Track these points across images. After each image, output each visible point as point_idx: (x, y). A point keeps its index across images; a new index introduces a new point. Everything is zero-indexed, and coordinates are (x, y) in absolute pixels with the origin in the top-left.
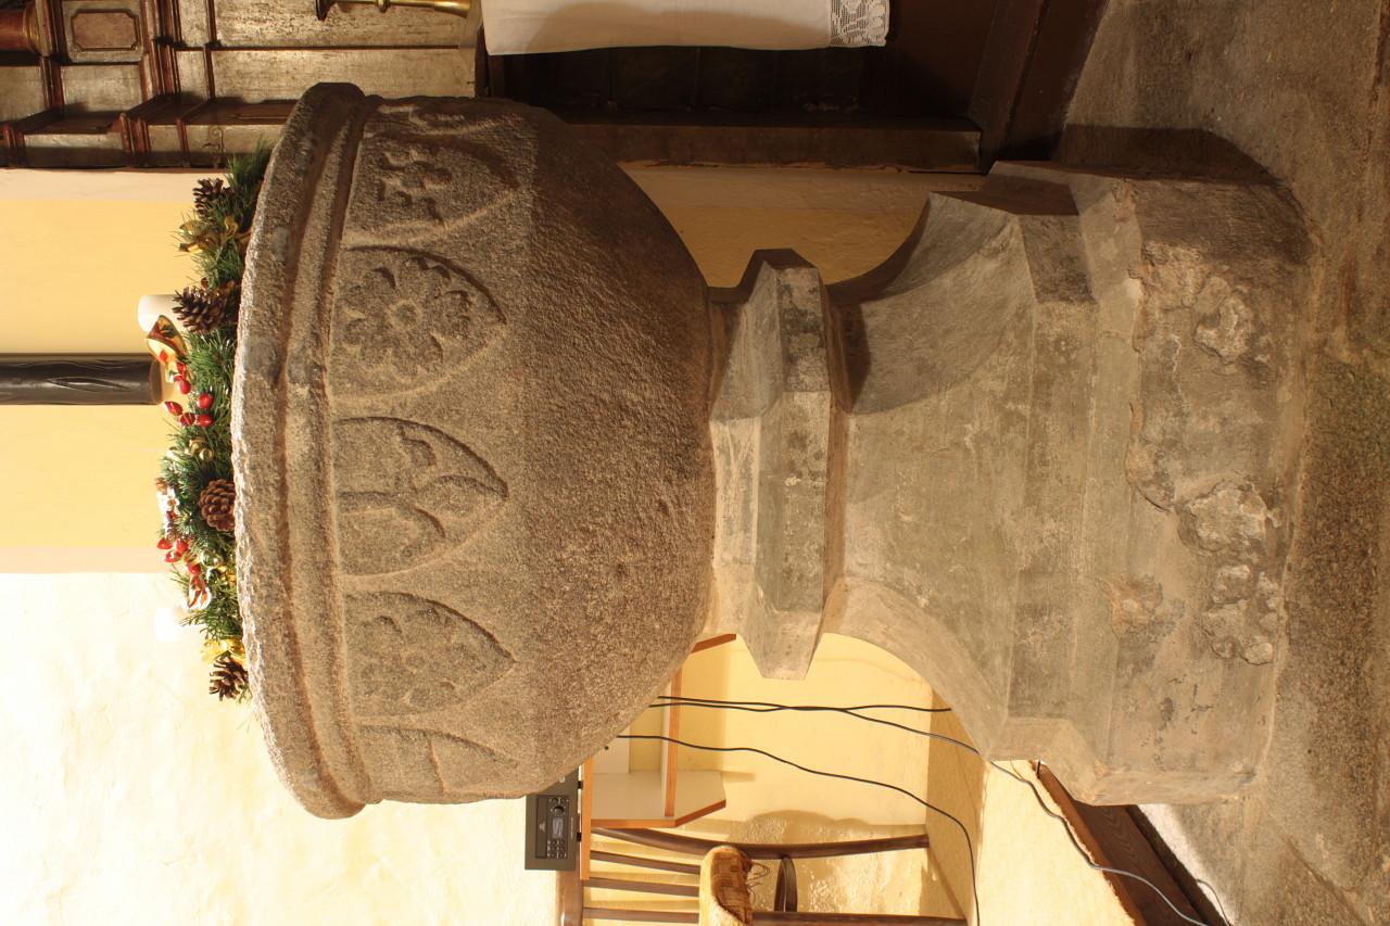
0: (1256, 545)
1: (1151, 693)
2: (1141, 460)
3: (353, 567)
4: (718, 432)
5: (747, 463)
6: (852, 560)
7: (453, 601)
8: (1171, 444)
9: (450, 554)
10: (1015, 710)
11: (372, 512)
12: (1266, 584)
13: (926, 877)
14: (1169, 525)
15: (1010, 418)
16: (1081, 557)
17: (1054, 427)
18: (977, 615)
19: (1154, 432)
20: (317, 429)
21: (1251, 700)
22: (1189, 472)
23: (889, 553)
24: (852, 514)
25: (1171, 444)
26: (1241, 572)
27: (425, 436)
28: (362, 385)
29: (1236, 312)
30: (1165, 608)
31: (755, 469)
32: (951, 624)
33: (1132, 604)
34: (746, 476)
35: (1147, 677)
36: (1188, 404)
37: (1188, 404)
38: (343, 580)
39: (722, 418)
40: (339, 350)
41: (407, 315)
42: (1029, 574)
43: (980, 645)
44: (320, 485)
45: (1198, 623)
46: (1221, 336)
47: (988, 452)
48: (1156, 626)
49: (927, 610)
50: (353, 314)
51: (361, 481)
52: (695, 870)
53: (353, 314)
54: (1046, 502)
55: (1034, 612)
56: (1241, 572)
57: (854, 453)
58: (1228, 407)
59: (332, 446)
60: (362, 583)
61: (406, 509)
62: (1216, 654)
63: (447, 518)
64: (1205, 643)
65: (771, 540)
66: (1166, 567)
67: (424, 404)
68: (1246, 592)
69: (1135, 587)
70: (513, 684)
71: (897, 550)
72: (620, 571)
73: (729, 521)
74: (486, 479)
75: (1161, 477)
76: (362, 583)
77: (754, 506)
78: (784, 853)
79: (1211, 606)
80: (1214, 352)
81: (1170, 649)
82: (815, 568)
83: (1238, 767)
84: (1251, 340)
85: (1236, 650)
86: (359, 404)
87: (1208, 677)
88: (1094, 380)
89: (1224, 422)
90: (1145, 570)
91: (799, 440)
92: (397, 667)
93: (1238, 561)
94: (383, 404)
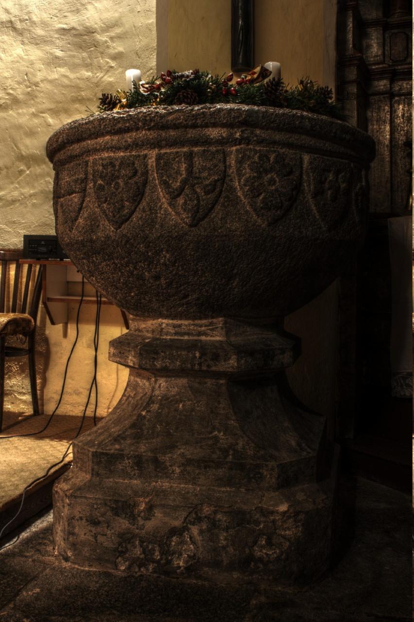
0: (169, 562)
1: (103, 515)
2: (207, 510)
3: (159, 158)
4: (219, 321)
5: (206, 334)
6: (162, 382)
7: (144, 203)
8: (214, 524)
9: (164, 201)
10: (95, 454)
11: (183, 167)
12: (151, 567)
13: (21, 414)
14: (177, 523)
15: (225, 452)
16: (165, 484)
17: (220, 472)
18: (138, 437)
19: (219, 516)
20: (222, 142)
21: (99, 560)
22: (201, 532)
23: (165, 398)
24: (183, 381)
25: (214, 524)
26: (157, 555)
27: (218, 190)
28: (240, 162)
29: (273, 553)
30: (141, 522)
31: (203, 338)
32: (133, 426)
33: (142, 507)
34: (200, 334)
35: (109, 513)
36: (232, 532)
37: (232, 532)
38: (154, 153)
39: (225, 323)
40: (256, 152)
41: (272, 182)
42: (156, 461)
43: (124, 439)
44: (195, 142)
45: (134, 536)
46: (262, 547)
47: (210, 442)
48: (133, 518)
49: (140, 415)
50: (272, 158)
51: (198, 162)
52: (23, 311)
53: (272, 158)
54: (188, 468)
55: (139, 462)
56: (157, 555)
57: (209, 383)
58: (231, 550)
59: (213, 149)
60: (152, 162)
61: (185, 182)
62: (120, 544)
63: (181, 201)
64: (126, 539)
65: (170, 345)
66: (159, 520)
67: (232, 190)
68: (148, 558)
69: (150, 508)
70: (107, 229)
71: (167, 401)
72: (157, 278)
73: (180, 326)
74: (199, 216)
75: (199, 519)
76: (152, 162)
77: (186, 337)
78: (31, 351)
79: (142, 542)
80: (255, 543)
81: (123, 524)
82: (158, 364)
83: (69, 554)
84: (260, 560)
85: (122, 553)
86: (232, 161)
87: (108, 540)
88: (243, 490)
89: (224, 548)
90: (158, 513)
91: (216, 358)
92: (114, 178)
93: (162, 554)
94: (232, 171)
